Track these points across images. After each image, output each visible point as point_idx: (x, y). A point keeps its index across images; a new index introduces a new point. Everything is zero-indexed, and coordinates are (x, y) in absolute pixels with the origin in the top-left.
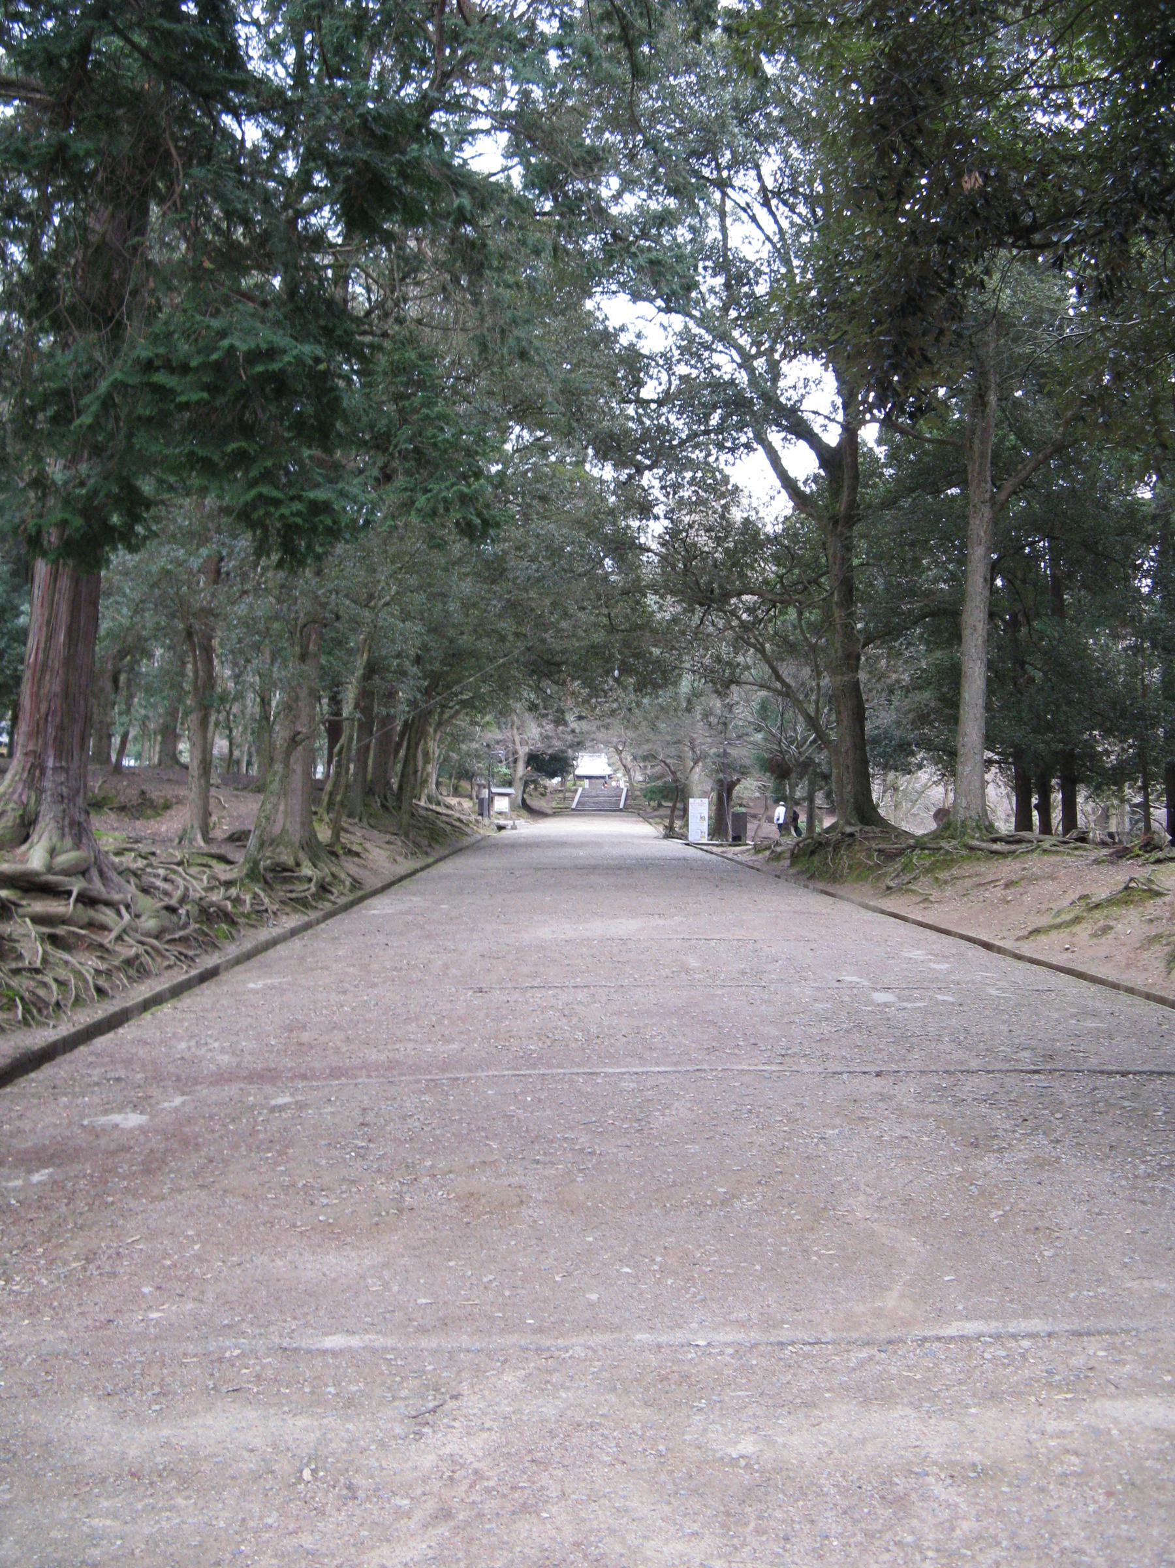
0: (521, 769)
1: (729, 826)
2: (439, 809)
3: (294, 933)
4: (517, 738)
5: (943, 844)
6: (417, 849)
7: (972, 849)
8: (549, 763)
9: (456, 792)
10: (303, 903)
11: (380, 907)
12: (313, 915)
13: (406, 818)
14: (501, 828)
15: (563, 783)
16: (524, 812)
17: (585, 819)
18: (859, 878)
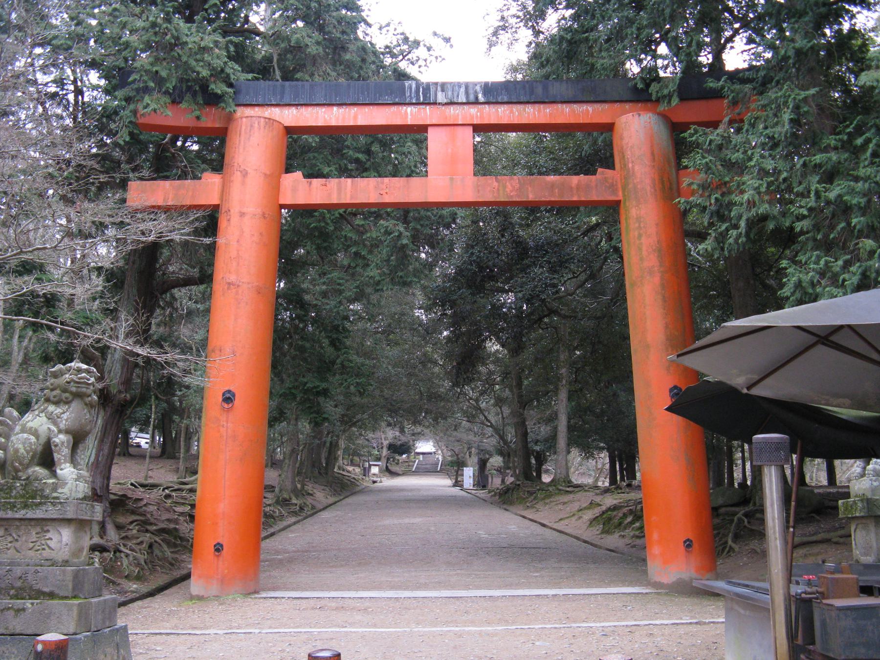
0: (385, 452)
1: (481, 481)
2: (344, 473)
3: (295, 523)
4: (383, 436)
5: (551, 489)
6: (335, 493)
7: (560, 490)
8: (399, 449)
9: (352, 464)
10: (295, 513)
11: (325, 515)
12: (300, 518)
13: (330, 479)
14: (374, 482)
15: (408, 457)
16: (387, 474)
17: (418, 477)
18: (520, 503)
